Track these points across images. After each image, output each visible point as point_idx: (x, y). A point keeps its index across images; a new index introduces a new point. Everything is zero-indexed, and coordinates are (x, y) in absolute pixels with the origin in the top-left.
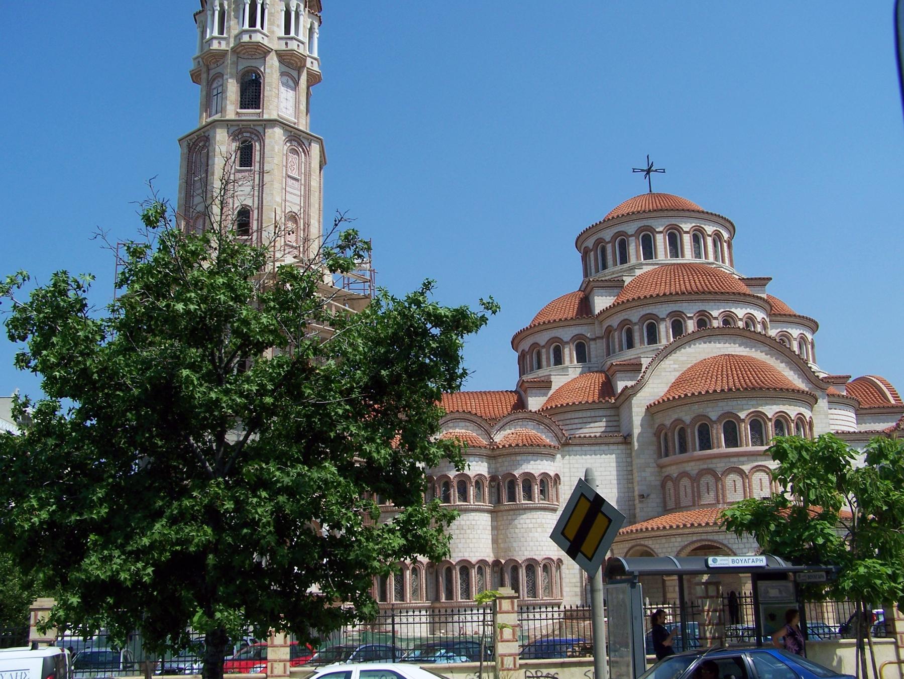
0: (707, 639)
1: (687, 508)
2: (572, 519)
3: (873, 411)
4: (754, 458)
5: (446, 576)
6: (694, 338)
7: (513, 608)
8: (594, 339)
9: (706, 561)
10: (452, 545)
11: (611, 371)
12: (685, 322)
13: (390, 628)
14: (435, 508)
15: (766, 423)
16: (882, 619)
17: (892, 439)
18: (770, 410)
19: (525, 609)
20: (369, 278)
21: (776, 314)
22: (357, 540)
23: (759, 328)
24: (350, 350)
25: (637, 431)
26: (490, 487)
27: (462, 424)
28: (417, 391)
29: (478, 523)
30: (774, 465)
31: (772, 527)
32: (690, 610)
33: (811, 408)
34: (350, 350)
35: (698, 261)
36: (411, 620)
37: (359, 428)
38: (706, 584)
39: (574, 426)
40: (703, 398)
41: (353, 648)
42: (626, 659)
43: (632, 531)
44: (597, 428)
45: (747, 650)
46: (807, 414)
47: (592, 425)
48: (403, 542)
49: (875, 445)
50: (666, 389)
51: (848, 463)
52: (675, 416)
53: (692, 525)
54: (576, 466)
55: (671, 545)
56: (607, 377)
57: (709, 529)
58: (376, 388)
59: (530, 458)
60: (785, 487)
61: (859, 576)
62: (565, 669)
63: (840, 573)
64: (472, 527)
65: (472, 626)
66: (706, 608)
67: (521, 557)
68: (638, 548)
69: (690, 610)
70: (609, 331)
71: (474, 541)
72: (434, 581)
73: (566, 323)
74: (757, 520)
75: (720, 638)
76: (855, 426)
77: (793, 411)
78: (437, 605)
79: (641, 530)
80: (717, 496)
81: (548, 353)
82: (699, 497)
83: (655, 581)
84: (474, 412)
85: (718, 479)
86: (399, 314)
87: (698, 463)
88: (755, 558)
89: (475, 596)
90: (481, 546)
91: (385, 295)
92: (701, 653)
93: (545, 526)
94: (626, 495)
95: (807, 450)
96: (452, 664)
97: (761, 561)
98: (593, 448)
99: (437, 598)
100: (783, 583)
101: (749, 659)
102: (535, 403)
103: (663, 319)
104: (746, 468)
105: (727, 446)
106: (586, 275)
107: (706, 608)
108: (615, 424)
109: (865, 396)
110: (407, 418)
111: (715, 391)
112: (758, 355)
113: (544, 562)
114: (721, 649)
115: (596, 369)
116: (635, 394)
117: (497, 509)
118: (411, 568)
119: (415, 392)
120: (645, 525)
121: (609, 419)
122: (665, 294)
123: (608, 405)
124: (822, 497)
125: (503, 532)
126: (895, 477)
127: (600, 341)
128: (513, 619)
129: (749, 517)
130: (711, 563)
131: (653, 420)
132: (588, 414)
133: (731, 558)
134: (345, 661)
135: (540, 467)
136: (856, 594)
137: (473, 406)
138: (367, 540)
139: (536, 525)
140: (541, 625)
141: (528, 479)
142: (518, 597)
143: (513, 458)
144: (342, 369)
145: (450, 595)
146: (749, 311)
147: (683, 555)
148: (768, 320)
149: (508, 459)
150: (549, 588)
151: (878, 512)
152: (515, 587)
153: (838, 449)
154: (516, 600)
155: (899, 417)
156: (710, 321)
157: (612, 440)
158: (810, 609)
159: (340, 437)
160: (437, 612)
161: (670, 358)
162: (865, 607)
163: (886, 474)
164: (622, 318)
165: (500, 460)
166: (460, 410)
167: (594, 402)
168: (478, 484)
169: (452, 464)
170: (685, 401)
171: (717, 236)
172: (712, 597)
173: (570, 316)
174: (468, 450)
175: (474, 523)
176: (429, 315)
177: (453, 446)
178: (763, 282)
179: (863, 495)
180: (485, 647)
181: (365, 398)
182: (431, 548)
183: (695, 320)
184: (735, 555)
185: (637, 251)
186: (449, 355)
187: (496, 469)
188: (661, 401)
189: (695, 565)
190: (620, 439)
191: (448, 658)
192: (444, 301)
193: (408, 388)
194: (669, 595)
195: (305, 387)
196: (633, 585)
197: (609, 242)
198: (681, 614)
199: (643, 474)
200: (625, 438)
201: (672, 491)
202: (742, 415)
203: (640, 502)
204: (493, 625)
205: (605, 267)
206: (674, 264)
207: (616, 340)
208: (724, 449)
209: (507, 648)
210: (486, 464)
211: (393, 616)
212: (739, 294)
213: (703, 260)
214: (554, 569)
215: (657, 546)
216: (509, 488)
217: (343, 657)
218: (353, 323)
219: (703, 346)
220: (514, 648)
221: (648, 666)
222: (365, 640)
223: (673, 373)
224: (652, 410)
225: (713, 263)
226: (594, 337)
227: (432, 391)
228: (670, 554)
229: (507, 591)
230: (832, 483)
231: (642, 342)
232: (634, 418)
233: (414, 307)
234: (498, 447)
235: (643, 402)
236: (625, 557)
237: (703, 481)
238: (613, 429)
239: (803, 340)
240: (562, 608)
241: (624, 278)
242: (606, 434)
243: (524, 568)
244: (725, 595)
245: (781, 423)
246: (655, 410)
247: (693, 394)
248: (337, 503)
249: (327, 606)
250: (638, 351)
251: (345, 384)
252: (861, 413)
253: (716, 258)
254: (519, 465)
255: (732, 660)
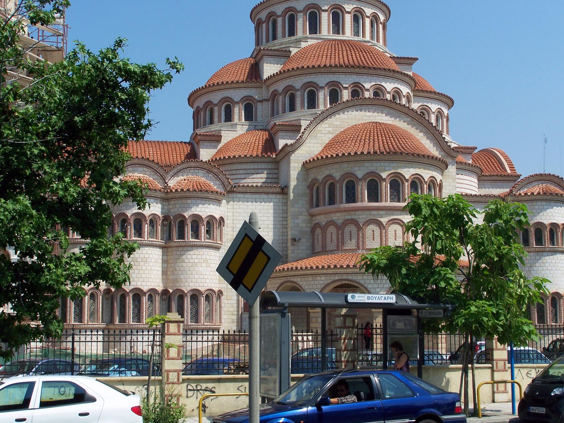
0: (342, 362)
1: (332, 252)
2: (234, 258)
3: (492, 178)
4: (391, 212)
5: (122, 303)
6: (348, 106)
7: (179, 331)
8: (261, 101)
9: (346, 297)
10: (133, 273)
11: (274, 130)
12: (341, 91)
13: (70, 345)
14: (117, 241)
15: (403, 183)
16: (483, 349)
17: (507, 203)
18: (408, 172)
19: (189, 332)
20: (62, 32)
21: (420, 90)
22: (47, 267)
23: (404, 101)
24: (46, 97)
25: (293, 183)
26: (163, 225)
27: (141, 169)
28: (107, 137)
29: (151, 256)
30: (408, 218)
31: (404, 271)
32: (329, 338)
33: (442, 172)
34: (46, 97)
35: (356, 38)
36: (89, 338)
37: (51, 167)
38: (345, 316)
39: (239, 176)
40: (352, 159)
41: (36, 362)
42: (273, 377)
43: (283, 269)
44: (259, 179)
45: (375, 372)
46: (438, 177)
47: (255, 176)
48: (88, 269)
49: (493, 207)
50: (320, 149)
51: (470, 220)
52: (327, 173)
53: (335, 266)
54: (238, 210)
55: (316, 283)
56: (270, 135)
57: (349, 271)
58: (70, 132)
59: (198, 202)
60: (416, 237)
61: (471, 315)
62: (222, 384)
63: (455, 311)
64: (145, 261)
65: (142, 346)
66: (343, 336)
67: (186, 288)
68: (288, 284)
69: (329, 338)
70: (275, 94)
71: (146, 272)
72: (110, 307)
73: (237, 85)
74: (392, 265)
75: (353, 362)
76: (477, 190)
77: (426, 174)
78: (111, 327)
79: (292, 268)
80: (358, 244)
81: (220, 111)
82: (343, 244)
83: (301, 313)
84: (151, 159)
85: (359, 228)
86: (93, 67)
87: (344, 214)
88: (386, 296)
89: (146, 320)
90: (153, 276)
91: (83, 48)
92: (337, 373)
93: (209, 261)
94: (281, 238)
95: (437, 207)
96: (123, 377)
97: (392, 299)
98: (254, 196)
99: (112, 321)
100: (408, 317)
101: (376, 379)
102: (206, 154)
103: (323, 88)
104: (384, 220)
105: (370, 200)
106: (258, 43)
107: (343, 336)
108: (274, 176)
109: (487, 165)
110: (96, 161)
111: (362, 153)
112: (401, 124)
113: (206, 293)
114: (354, 370)
115: (261, 128)
116: (293, 151)
117: (167, 245)
118: (89, 294)
119: (104, 138)
120: (295, 264)
121: (269, 171)
122: (325, 66)
123: (270, 160)
124: (446, 247)
125: (172, 265)
126: (506, 234)
127: (266, 103)
128: (178, 340)
129: (385, 261)
130: (350, 299)
131: (307, 174)
132: (252, 166)
133: (366, 295)
134: (28, 373)
135: (207, 210)
136: (467, 329)
137: (152, 154)
138: (56, 266)
139: (202, 261)
140: (202, 347)
141: (196, 221)
142: (183, 322)
143: (184, 201)
144: (39, 114)
145: (123, 319)
146: (396, 85)
147: (326, 291)
148: (412, 95)
149: (180, 202)
150: (210, 315)
151: (490, 263)
152: (181, 312)
153: (463, 208)
154: (182, 324)
155: (513, 184)
156: (363, 92)
157: (271, 190)
158: (428, 339)
159: (34, 175)
160: (112, 332)
161: (326, 122)
162: (471, 339)
163: (499, 232)
164: (287, 84)
165: (172, 202)
166: (140, 156)
167: (257, 156)
168: (152, 223)
169: (135, 203)
170: (336, 160)
171: (375, 18)
172: (349, 327)
173: (241, 79)
174: (149, 193)
175: (147, 256)
176: (120, 69)
177: (136, 188)
178: (410, 61)
179: (480, 247)
180: (154, 364)
181: (59, 140)
182: (113, 275)
183: (350, 90)
184: (369, 292)
185: (304, 26)
186: (136, 106)
187: (169, 210)
188: (315, 159)
189: (337, 300)
190: (278, 190)
191: (120, 372)
192: (134, 57)
193: (98, 134)
194: (312, 325)
195: (5, 128)
196: (283, 315)
197: (280, 16)
198: (322, 341)
199: (296, 221)
200: (283, 189)
201: (320, 237)
202: (384, 175)
203: (292, 245)
204: (161, 345)
205: (275, 38)
206: (335, 40)
207: (280, 103)
208: (366, 203)
209: (173, 365)
210: (160, 205)
211: (73, 335)
212: (389, 70)
213: (360, 38)
214: (215, 299)
215: (305, 283)
216: (179, 227)
217: (26, 370)
218: (51, 72)
219: (355, 113)
220: (179, 365)
221: (292, 383)
222: (46, 355)
223: (327, 135)
224: (307, 166)
225: (369, 42)
226: (261, 99)
227: (119, 137)
228: (315, 289)
229: (174, 316)
230: (455, 236)
231: (302, 106)
232: (291, 172)
233: (106, 63)
234: (171, 191)
235: (300, 158)
236: (277, 290)
237: (347, 229)
238: (273, 181)
239: (440, 113)
240: (221, 332)
241: (291, 49)
242: (267, 185)
243: (189, 297)
244: (360, 326)
245: (416, 183)
246: (310, 166)
247: (343, 154)
248: (30, 233)
249: (17, 323)
250: (299, 115)
251: (42, 127)
252: (482, 179)
253: (372, 37)
254: (189, 207)
255: (362, 380)
